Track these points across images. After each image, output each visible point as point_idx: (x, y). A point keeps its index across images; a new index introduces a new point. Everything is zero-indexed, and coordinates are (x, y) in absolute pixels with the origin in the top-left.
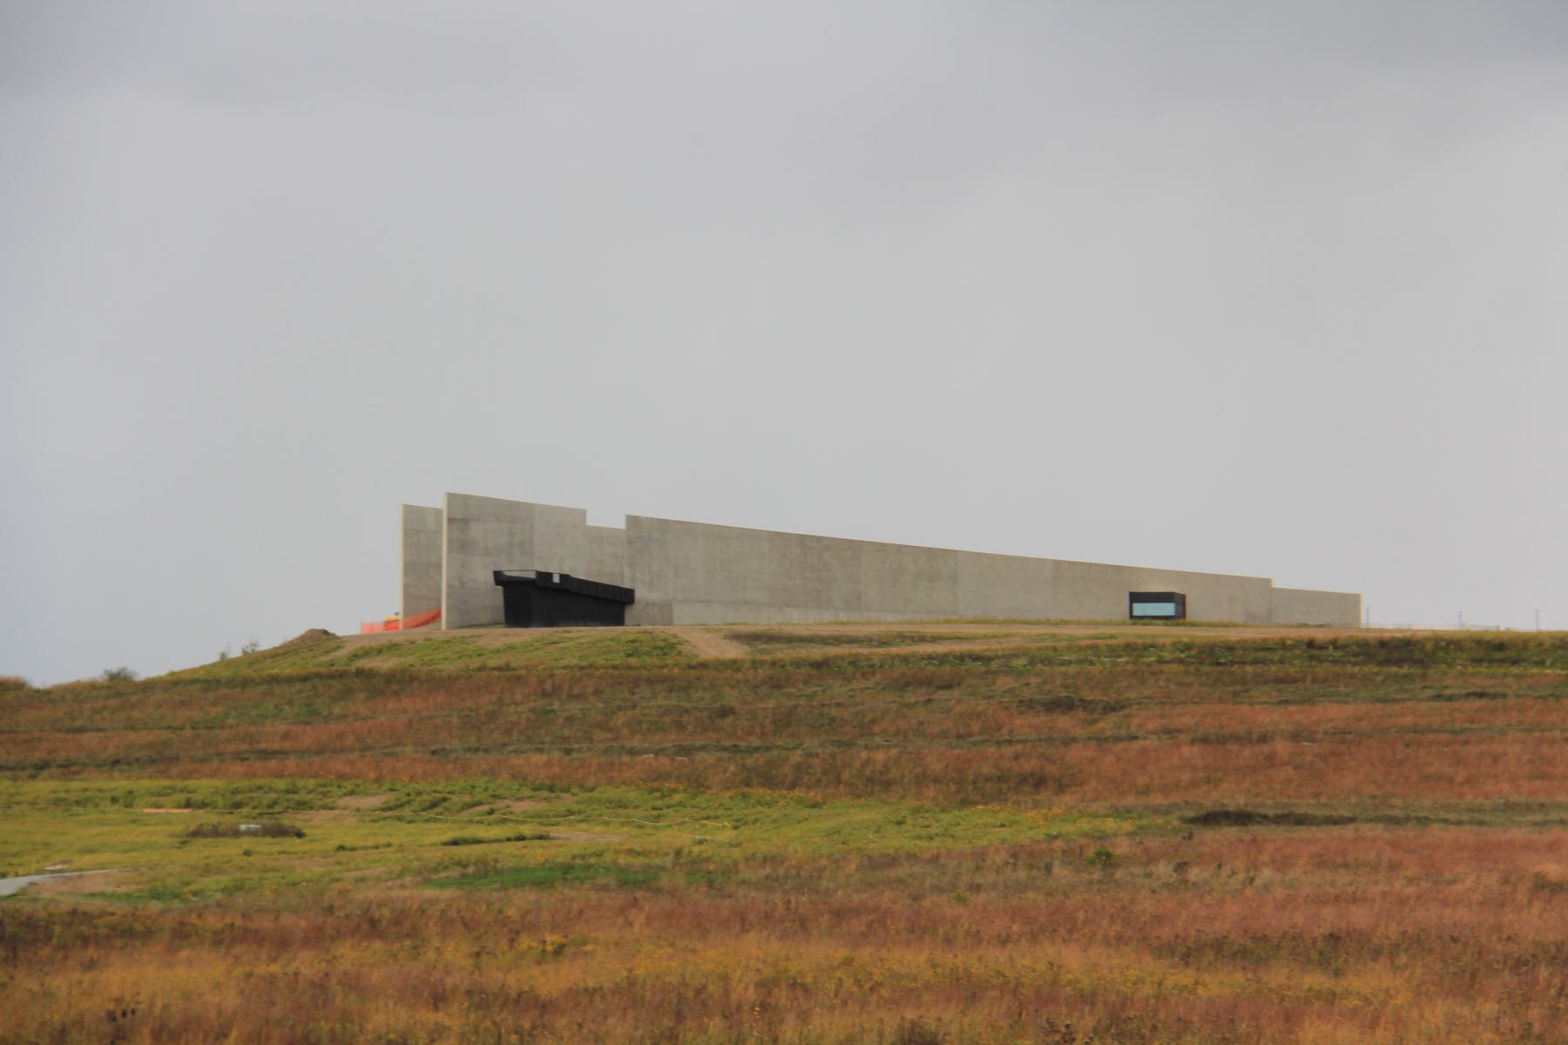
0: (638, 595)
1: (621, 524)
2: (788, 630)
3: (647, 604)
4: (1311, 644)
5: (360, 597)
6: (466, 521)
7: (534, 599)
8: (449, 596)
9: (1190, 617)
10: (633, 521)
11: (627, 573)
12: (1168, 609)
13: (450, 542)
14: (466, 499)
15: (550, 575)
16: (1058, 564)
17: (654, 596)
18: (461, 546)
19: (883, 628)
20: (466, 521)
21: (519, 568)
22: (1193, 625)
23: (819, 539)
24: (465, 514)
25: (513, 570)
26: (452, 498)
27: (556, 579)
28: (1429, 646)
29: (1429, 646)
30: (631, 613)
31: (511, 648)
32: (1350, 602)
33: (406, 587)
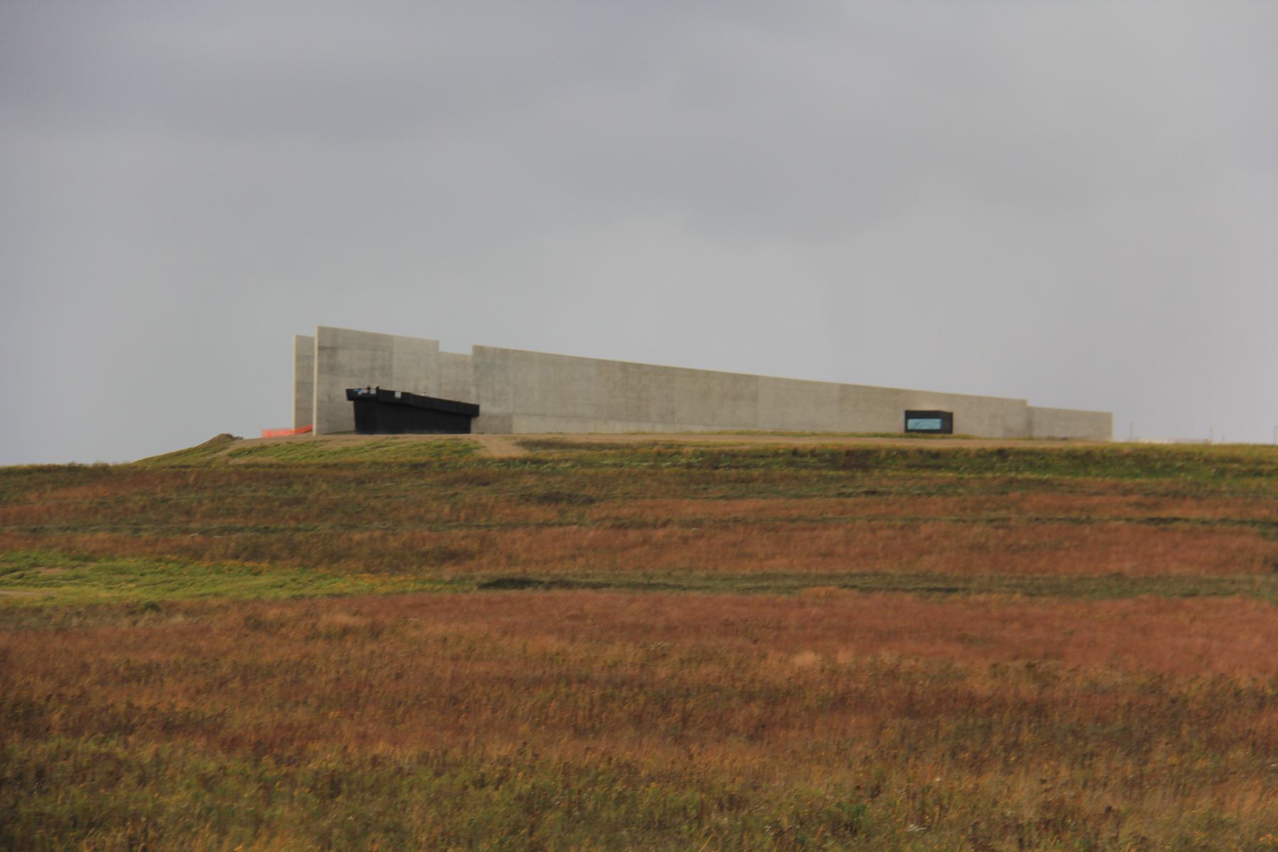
0: (482, 409)
1: (469, 351)
2: (569, 439)
3: (490, 417)
4: (795, 452)
5: (261, 406)
6: (334, 349)
7: (379, 410)
8: (319, 408)
9: (956, 431)
10: (479, 351)
11: (473, 390)
12: (935, 424)
13: (320, 365)
14: (335, 333)
15: (392, 393)
16: (844, 388)
17: (496, 410)
18: (330, 369)
19: (838, 441)
20: (334, 349)
21: (363, 384)
22: (958, 437)
23: (639, 366)
24: (331, 346)
25: (382, 388)
26: (322, 331)
27: (398, 395)
28: (883, 454)
29: (883, 454)
30: (475, 424)
31: (347, 450)
32: (1104, 420)
33: (297, 401)
